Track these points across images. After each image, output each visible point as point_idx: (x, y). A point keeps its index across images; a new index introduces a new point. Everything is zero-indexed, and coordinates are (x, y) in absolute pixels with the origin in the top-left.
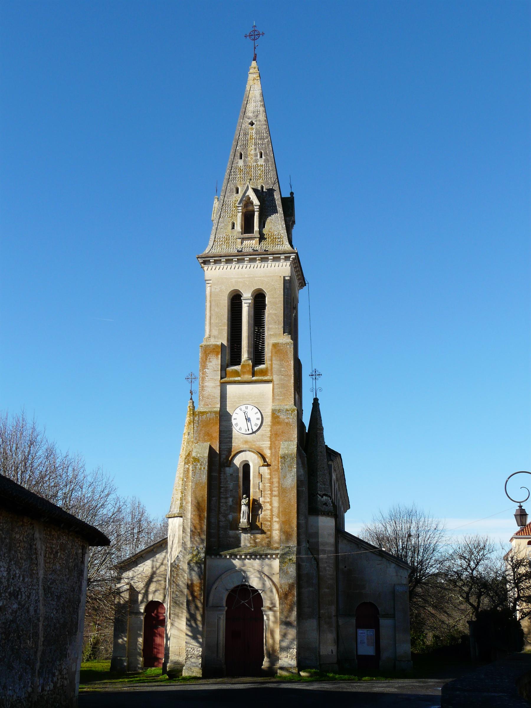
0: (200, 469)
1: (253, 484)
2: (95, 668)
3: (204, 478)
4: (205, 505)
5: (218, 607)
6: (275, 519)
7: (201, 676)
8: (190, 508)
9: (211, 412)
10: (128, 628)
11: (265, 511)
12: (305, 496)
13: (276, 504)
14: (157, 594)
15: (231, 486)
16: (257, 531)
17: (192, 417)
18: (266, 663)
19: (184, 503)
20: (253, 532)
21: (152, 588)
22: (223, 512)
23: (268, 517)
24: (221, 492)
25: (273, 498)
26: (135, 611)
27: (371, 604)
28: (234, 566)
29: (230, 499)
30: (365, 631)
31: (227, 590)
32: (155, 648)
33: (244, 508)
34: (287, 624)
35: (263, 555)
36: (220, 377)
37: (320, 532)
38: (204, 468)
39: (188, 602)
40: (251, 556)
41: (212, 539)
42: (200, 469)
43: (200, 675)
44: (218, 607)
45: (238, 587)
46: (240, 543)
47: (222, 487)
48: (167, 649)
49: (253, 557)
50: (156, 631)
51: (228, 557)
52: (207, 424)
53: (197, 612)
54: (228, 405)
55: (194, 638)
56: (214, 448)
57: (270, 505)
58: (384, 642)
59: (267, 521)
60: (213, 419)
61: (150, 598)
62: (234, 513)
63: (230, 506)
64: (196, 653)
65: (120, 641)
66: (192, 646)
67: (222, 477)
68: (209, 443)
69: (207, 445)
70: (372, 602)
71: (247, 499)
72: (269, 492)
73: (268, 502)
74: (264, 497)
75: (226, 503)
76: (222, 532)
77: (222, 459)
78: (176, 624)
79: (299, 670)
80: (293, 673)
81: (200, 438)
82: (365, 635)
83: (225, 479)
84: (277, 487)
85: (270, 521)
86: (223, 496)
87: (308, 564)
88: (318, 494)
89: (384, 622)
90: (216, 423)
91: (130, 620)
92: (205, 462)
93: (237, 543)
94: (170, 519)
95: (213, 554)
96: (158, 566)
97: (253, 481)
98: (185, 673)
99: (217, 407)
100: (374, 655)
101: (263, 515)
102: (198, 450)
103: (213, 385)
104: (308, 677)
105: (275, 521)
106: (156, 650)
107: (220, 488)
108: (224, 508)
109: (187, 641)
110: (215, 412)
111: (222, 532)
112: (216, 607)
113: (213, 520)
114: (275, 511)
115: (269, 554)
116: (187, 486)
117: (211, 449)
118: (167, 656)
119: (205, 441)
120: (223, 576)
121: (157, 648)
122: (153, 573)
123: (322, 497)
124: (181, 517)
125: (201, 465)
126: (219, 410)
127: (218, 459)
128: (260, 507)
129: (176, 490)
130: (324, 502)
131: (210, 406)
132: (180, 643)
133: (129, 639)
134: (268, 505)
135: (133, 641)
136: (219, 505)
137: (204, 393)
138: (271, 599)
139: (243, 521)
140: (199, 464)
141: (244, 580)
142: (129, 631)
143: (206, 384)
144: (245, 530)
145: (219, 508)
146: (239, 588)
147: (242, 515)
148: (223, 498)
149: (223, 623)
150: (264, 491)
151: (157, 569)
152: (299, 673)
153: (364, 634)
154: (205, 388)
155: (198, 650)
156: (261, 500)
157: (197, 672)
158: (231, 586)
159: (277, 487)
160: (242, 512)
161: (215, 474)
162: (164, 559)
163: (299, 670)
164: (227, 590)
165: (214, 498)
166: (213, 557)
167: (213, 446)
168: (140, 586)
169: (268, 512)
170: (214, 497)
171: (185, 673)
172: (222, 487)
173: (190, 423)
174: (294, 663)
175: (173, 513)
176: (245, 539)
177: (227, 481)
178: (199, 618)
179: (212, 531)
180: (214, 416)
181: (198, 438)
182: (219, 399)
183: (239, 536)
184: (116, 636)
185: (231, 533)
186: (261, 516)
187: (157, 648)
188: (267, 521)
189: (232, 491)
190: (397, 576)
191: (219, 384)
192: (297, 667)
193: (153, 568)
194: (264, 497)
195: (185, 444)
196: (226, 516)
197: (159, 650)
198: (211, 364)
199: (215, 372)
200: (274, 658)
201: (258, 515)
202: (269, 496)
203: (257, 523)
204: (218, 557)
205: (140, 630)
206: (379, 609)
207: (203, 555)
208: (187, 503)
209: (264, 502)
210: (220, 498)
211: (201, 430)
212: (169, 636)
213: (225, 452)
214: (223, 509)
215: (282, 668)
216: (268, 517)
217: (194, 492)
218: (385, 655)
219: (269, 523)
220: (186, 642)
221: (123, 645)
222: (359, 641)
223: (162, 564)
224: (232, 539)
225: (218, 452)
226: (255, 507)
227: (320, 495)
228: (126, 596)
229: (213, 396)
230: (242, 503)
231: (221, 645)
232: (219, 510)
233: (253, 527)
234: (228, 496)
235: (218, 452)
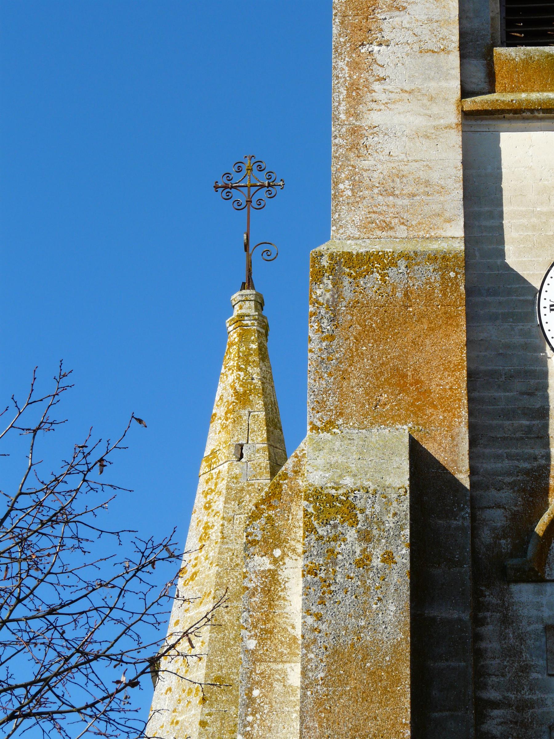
0: (364, 562)
2: (356, 92)
3: (391, 617)
9: (411, 258)
17: (255, 371)
36: (455, 85)
38: (388, 558)
42: (364, 562)
47: (495, 705)
52: (388, 320)
54: (509, 234)
56: (441, 457)
60: (429, 297)
67: (492, 645)
68: (406, 428)
69: (398, 436)
77: (486, 536)
81: (343, 397)
83: (511, 653)
90: (450, 317)
92: (390, 522)
99: (452, 235)
102: (337, 458)
103: (419, 122)
110: (441, 260)
116: (266, 682)
117: (423, 465)
119: (377, 416)
125: (365, 537)
126: (460, 246)
127: (463, 520)
131: (402, 232)
137: (366, 164)
140: (351, 534)
143: (375, 118)
154: (371, 141)
161: (452, 613)
167: (431, 447)
172: (495, 705)
173: (242, 399)
177: (526, 669)
180: (435, 278)
181: (331, 401)
182: (459, 193)
191: (453, 117)
195: (219, 505)
198: (399, 19)
199: (429, 58)
211: (351, 358)
213: (505, 495)
225: (464, 479)
229: (417, 182)
235: (464, 479)
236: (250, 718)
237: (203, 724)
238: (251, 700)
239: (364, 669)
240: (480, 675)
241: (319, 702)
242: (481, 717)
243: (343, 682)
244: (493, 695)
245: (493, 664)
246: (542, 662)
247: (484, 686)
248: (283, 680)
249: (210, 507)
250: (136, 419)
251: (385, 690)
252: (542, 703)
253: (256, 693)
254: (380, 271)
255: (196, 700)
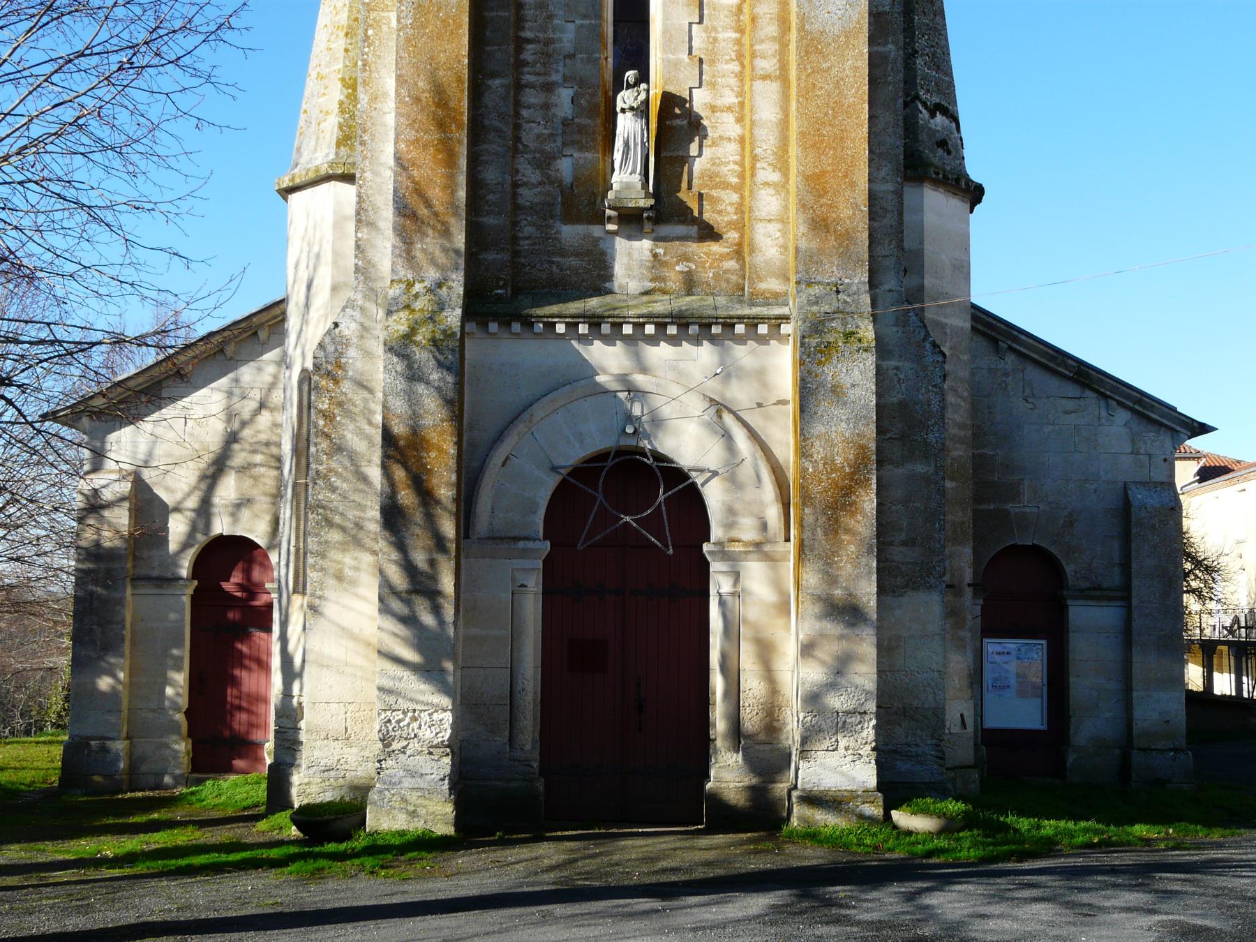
1: (666, 31)
4: (461, 102)
5: (516, 539)
6: (767, 174)
7: (450, 830)
8: (390, 120)
10: (127, 633)
11: (714, 144)
12: (895, 77)
13: (767, 108)
14: (245, 514)
15: (567, 35)
16: (681, 229)
18: (728, 774)
19: (364, 98)
20: (665, 230)
21: (228, 489)
22: (532, 145)
23: (729, 172)
24: (524, 63)
25: (758, 85)
26: (155, 573)
27: (1036, 551)
28: (587, 371)
29: (565, 95)
30: (1011, 645)
31: (554, 469)
32: (240, 708)
33: (626, 125)
34: (845, 612)
35: (716, 320)
37: (928, 248)
39: (392, 517)
40: (661, 327)
41: (490, 256)
43: (445, 829)
44: (516, 539)
45: (602, 457)
46: (609, 277)
47: (529, 41)
48: (289, 716)
49: (672, 330)
50: (245, 649)
51: (561, 328)
53: (440, 558)
55: (428, 670)
57: (740, 120)
58: (1082, 685)
59: (726, 186)
61: (221, 526)
62: (583, 148)
63: (566, 122)
64: (426, 734)
65: (104, 683)
66: (412, 706)
70: (1044, 545)
71: (643, 86)
72: (735, 66)
73: (729, 109)
74: (713, 85)
75: (546, 106)
76: (528, 230)
78: (330, 609)
79: (888, 807)
80: (861, 816)
82: (1017, 660)
84: (773, 39)
85: (739, 188)
86: (531, 78)
87: (908, 365)
88: (917, 97)
89: (1082, 615)
91: (133, 604)
93: (597, 277)
94: (294, 197)
95: (496, 317)
96: (246, 415)
97: (666, 17)
98: (383, 820)
100: (1044, 727)
101: (711, 160)
104: (930, 835)
105: (767, 184)
106: (244, 717)
107: (520, 43)
108: (537, 129)
109: (387, 683)
111: (528, 230)
112: (506, 540)
113: (491, 175)
114: (767, 141)
115: (741, 318)
116: (377, 24)
118: (289, 743)
120: (539, 411)
121: (249, 711)
122: (232, 438)
123: (933, 115)
124: (349, 178)
128: (695, 126)
129: (320, 77)
130: (939, 137)
132: (355, 692)
133: (132, 674)
134: (729, 118)
135: (147, 682)
136: (517, 115)
138: (739, 506)
139: (627, 180)
141: (629, 430)
142: (133, 643)
144: (632, 221)
145: (517, 127)
146: (610, 463)
147: (618, 156)
148: (530, 86)
149: (532, 608)
150: (712, 62)
151: (244, 424)
152: (887, 817)
153: (1005, 658)
155: (435, 717)
156: (700, 101)
157: (439, 816)
158: (574, 455)
159: (773, 39)
160: (619, 144)
162: (272, 386)
163: (888, 807)
164: (554, 469)
165: (497, 82)
166: (493, 327)
168: (176, 485)
169: (730, 151)
170: (494, 75)
171: (383, 820)
172: (529, 41)
174: (865, 775)
175: (312, 166)
176: (631, 258)
177: (550, 17)
178: (447, 583)
179: (490, 221)
183: (602, 245)
184: (84, 663)
185: (570, 233)
186: (698, 166)
187: (249, 711)
188: (726, 186)
189: (571, 56)
190: (1135, 452)
192: (880, 787)
193: (230, 415)
194: (713, 85)
196: (545, 162)
197: (257, 715)
200: (767, 757)
201: (685, 160)
202: (733, 81)
203: (682, 195)
204: (516, 327)
205: (179, 645)
206: (1069, 569)
207: (453, 317)
208: (374, 99)
209: (713, 109)
210: (519, 86)
212: (297, 661)
214: (532, 132)
215: (814, 799)
216: (729, 172)
217: (408, 44)
218: (1092, 726)
219: (735, 197)
220: (381, 689)
221: (114, 694)
222: (988, 676)
223: (262, 406)
224: (573, 261)
226: (676, 126)
227: (925, 104)
228: (121, 518)
230: (620, 105)
231: (529, 698)
232: (518, 139)
233: (669, 210)
234: (556, 77)
236: (366, 50)
237: (346, 50)
238: (367, 37)
239: (438, 17)
240: (520, 21)
241: (408, 40)
242: (519, 49)
243: (424, 27)
244: (528, 34)
245: (529, 13)
246: (561, 13)
247: (523, 29)
248: (388, 24)
249: (833, 392)
250: (1140, 749)
251: (452, 33)
252: (560, 40)
253: (370, 32)
254: (422, 336)
255: (342, 34)
